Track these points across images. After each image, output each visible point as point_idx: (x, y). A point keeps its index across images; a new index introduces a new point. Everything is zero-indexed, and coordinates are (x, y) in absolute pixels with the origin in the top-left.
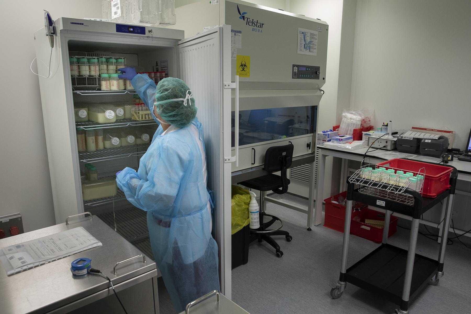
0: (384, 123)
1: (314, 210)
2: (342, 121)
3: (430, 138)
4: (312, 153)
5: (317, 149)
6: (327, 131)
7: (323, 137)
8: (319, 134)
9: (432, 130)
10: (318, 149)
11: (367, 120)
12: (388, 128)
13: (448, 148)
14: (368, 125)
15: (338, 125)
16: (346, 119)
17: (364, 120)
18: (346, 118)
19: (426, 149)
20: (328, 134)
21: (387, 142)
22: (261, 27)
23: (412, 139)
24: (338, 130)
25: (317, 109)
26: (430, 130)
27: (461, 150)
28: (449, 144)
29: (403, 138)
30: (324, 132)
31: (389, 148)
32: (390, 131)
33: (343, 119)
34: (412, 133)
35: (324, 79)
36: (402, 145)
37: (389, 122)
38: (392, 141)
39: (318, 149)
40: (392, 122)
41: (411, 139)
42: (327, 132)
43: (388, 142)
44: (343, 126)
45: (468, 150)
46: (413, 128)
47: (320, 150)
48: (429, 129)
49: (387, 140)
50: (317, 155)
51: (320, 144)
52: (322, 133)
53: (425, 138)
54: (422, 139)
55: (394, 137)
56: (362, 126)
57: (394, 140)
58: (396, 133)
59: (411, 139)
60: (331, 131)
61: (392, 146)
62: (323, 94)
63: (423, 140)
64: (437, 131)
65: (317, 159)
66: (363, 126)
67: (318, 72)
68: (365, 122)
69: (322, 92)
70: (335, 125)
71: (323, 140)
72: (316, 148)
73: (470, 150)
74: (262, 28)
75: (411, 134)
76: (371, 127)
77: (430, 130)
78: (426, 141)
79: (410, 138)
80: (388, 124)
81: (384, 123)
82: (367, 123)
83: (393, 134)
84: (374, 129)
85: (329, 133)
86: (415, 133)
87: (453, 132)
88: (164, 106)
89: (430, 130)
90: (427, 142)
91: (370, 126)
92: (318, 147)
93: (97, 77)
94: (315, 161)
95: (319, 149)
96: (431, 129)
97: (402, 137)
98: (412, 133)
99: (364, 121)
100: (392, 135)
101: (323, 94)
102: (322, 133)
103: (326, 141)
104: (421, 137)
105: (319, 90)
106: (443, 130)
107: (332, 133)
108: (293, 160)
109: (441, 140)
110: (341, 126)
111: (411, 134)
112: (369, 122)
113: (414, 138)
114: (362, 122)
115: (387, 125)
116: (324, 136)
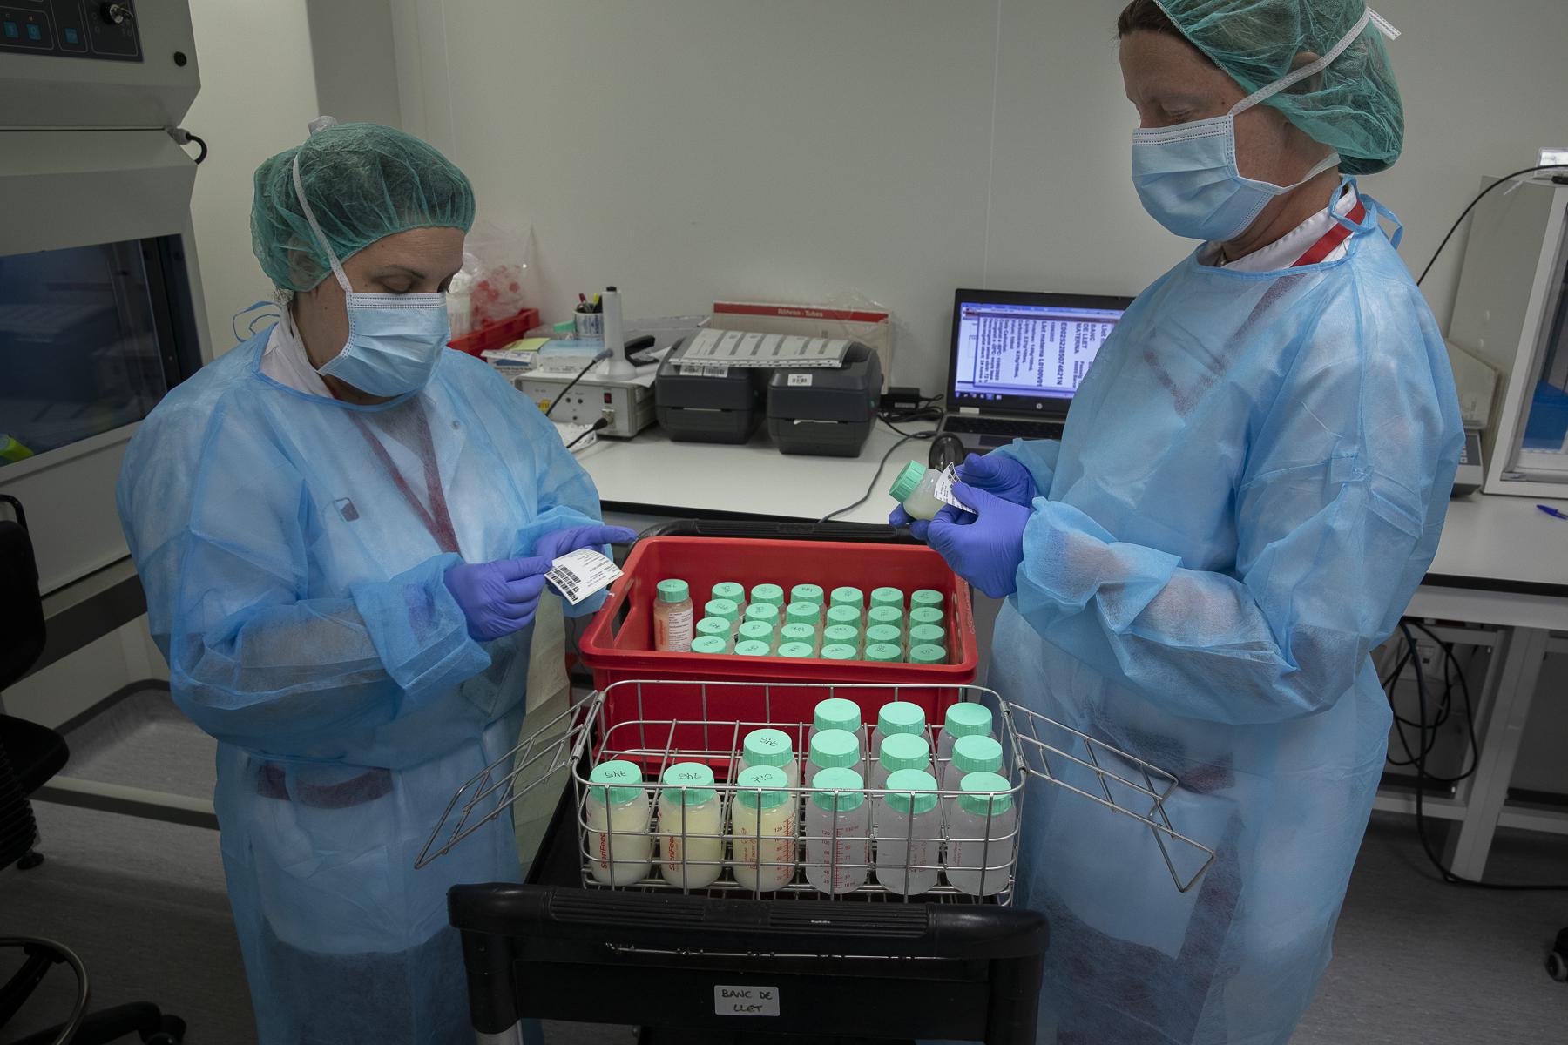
0: (582, 298)
3: (805, 363)
9: (802, 310)
11: (502, 285)
12: (602, 318)
13: (880, 391)
14: (512, 311)
17: (483, 286)
19: (793, 420)
21: (608, 399)
22: (1080, 363)
25: (180, 256)
26: (795, 313)
27: (923, 394)
28: (882, 376)
29: (682, 373)
31: (623, 426)
32: (614, 339)
34: (719, 340)
35: (180, 59)
36: (681, 408)
37: (606, 294)
38: (633, 389)
40: (619, 291)
41: (721, 372)
43: (613, 397)
45: (958, 395)
46: (719, 308)
48: (786, 309)
49: (609, 388)
53: (784, 364)
54: (774, 369)
55: (637, 363)
56: (480, 318)
57: (640, 386)
58: (648, 342)
61: (639, 413)
62: (199, 161)
63: (777, 376)
64: (821, 315)
66: (484, 321)
67: (114, 7)
68: (494, 295)
69: (193, 149)
73: (962, 394)
74: (1077, 363)
75: (716, 346)
76: (527, 317)
77: (795, 313)
78: (793, 380)
79: (715, 370)
80: (600, 299)
81: (582, 298)
82: (501, 300)
83: (637, 347)
84: (542, 324)
86: (736, 340)
87: (886, 316)
88: (274, 167)
89: (792, 316)
90: (795, 384)
91: (523, 311)
96: (796, 309)
97: (678, 368)
98: (719, 340)
99: (485, 293)
100: (627, 357)
101: (199, 161)
104: (764, 359)
105: (172, 141)
106: (844, 308)
108: (50, 610)
109: (858, 369)
111: (716, 346)
112: (511, 294)
113: (732, 370)
114: (473, 296)
115: (598, 308)
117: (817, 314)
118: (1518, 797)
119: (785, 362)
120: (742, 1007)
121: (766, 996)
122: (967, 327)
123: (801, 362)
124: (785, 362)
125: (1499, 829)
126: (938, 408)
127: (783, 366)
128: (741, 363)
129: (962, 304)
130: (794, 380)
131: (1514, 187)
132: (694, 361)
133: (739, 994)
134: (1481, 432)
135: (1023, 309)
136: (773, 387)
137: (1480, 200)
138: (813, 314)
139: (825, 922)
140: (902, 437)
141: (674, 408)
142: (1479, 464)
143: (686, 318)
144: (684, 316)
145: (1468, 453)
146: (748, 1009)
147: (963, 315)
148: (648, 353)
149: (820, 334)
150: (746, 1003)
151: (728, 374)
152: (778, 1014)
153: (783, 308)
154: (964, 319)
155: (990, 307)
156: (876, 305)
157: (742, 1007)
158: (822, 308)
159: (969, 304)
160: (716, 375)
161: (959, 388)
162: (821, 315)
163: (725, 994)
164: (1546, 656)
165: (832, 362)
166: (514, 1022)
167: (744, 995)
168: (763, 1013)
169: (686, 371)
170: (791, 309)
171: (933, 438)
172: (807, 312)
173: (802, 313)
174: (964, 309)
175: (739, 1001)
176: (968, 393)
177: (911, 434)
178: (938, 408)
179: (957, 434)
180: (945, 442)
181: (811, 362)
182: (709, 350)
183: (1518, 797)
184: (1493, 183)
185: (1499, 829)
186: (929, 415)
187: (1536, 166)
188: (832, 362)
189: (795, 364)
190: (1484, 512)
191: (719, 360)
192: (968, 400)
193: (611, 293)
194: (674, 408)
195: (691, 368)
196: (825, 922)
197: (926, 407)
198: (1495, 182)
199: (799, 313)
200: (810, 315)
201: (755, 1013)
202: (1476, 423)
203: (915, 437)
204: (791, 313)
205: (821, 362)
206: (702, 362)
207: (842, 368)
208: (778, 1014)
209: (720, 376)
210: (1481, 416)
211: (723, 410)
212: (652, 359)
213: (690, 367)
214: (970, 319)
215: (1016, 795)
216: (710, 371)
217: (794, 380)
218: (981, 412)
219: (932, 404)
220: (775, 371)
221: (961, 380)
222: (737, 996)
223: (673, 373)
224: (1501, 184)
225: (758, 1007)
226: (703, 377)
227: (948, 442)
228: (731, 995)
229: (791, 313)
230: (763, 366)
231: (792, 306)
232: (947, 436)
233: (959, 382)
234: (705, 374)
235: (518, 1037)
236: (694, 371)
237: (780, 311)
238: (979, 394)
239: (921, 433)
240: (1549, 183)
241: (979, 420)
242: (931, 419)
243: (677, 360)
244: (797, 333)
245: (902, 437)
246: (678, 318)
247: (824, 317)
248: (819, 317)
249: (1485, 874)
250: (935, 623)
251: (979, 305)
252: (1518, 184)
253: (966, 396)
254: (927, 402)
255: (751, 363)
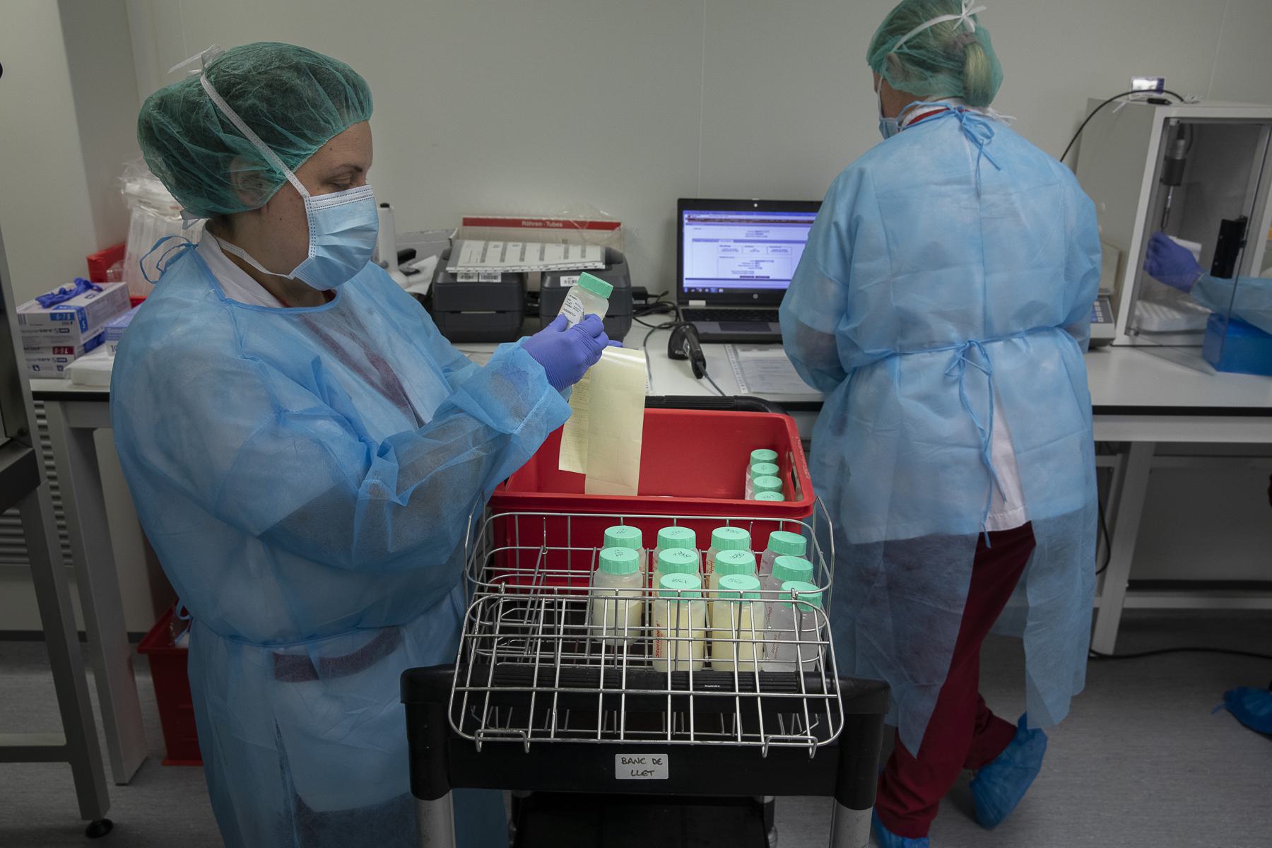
1: (90, 679)
2: (132, 221)
4: (12, 439)
5: (37, 406)
6: (63, 292)
7: (53, 334)
8: (22, 318)
10: (41, 407)
15: (110, 242)
16: (150, 211)
18: (148, 205)
20: (80, 310)
23: (499, 280)
24: (118, 277)
27: (650, 293)
29: (459, 280)
30: (48, 302)
33: (136, 215)
34: (485, 250)
36: (459, 312)
39: (41, 402)
40: (392, 207)
41: (495, 277)
42: (65, 295)
44: (137, 247)
45: (686, 291)
47: (54, 407)
50: (48, 458)
51: (42, 373)
52: (36, 309)
53: (553, 268)
59: (495, 277)
60: (88, 286)
64: (561, 225)
65: (44, 433)
70: (92, 247)
71: (57, 350)
72: (29, 402)
73: (690, 289)
77: (537, 224)
79: (489, 276)
85: (81, 301)
87: (618, 225)
89: (535, 227)
92: (38, 395)
93: (987, 114)
94: (44, 481)
95: (48, 404)
96: (538, 221)
97: (454, 275)
98: (485, 250)
102: (36, 309)
103: (76, 351)
107: (97, 302)
110: (131, 249)
113: (505, 275)
116: (58, 324)
117: (557, 225)
118: (1135, 585)
119: (554, 266)
120: (637, 771)
121: (658, 762)
122: (690, 231)
123: (569, 266)
124: (554, 266)
125: (1125, 611)
126: (669, 302)
127: (552, 270)
128: (513, 268)
129: (684, 212)
130: (565, 282)
131: (1119, 107)
132: (469, 269)
133: (635, 760)
134: (1109, 297)
135: (737, 214)
136: (545, 288)
137: (1094, 116)
138: (553, 224)
139: (716, 686)
140: (650, 329)
141: (452, 312)
142: (1111, 322)
143: (431, 232)
144: (428, 231)
145: (1103, 314)
146: (642, 774)
147: (686, 221)
148: (410, 265)
149: (561, 241)
150: (639, 768)
151: (502, 279)
152: (560, 469)
153: (526, 220)
154: (687, 224)
155: (708, 214)
156: (606, 215)
157: (637, 771)
158: (561, 219)
159: (690, 212)
160: (491, 281)
161: (686, 284)
162: (561, 225)
163: (624, 761)
164: (1151, 472)
165: (596, 264)
166: (448, 791)
167: (640, 761)
168: (655, 776)
169: (462, 277)
170: (533, 221)
171: (673, 328)
172: (548, 223)
173: (544, 224)
174: (686, 216)
175: (637, 767)
176: (695, 288)
177: (656, 325)
178: (669, 302)
179: (693, 323)
180: (684, 330)
181: (577, 265)
182: (479, 257)
183: (1135, 585)
184: (1100, 105)
185: (1125, 611)
186: (661, 309)
187: (1130, 91)
188: (596, 264)
189: (564, 268)
190: (1115, 356)
191: (493, 267)
192: (696, 294)
193: (385, 209)
194: (452, 312)
195: (467, 275)
196: (716, 686)
197: (657, 302)
198: (1103, 103)
199: (541, 224)
200: (551, 225)
201: (649, 777)
202: (1106, 290)
203: (660, 328)
204: (533, 224)
205: (586, 265)
206: (477, 269)
207: (606, 270)
208: (560, 469)
209: (495, 281)
210: (1108, 284)
211: (498, 312)
212: (414, 270)
213: (465, 274)
214: (691, 224)
215: (825, 593)
216: (485, 277)
217: (565, 282)
218: (707, 304)
219: (662, 299)
220: (546, 274)
221: (687, 277)
222: (634, 763)
223: (451, 280)
224: (1106, 105)
225: (651, 772)
226: (478, 283)
227: (687, 330)
228: (629, 762)
229: (533, 224)
230: (534, 270)
231: (535, 218)
232: (685, 325)
233: (687, 279)
234: (481, 280)
235: (450, 813)
236: (470, 277)
237: (523, 223)
238: (704, 289)
239: (665, 324)
240: (1145, 103)
241: (707, 310)
242: (664, 311)
243: (453, 269)
244: (533, 241)
245: (650, 329)
246: (422, 232)
247: (564, 227)
248: (559, 227)
249: (1116, 648)
250: (771, 462)
251: (698, 212)
252: (1122, 105)
253: (693, 291)
254: (656, 299)
255: (522, 268)
